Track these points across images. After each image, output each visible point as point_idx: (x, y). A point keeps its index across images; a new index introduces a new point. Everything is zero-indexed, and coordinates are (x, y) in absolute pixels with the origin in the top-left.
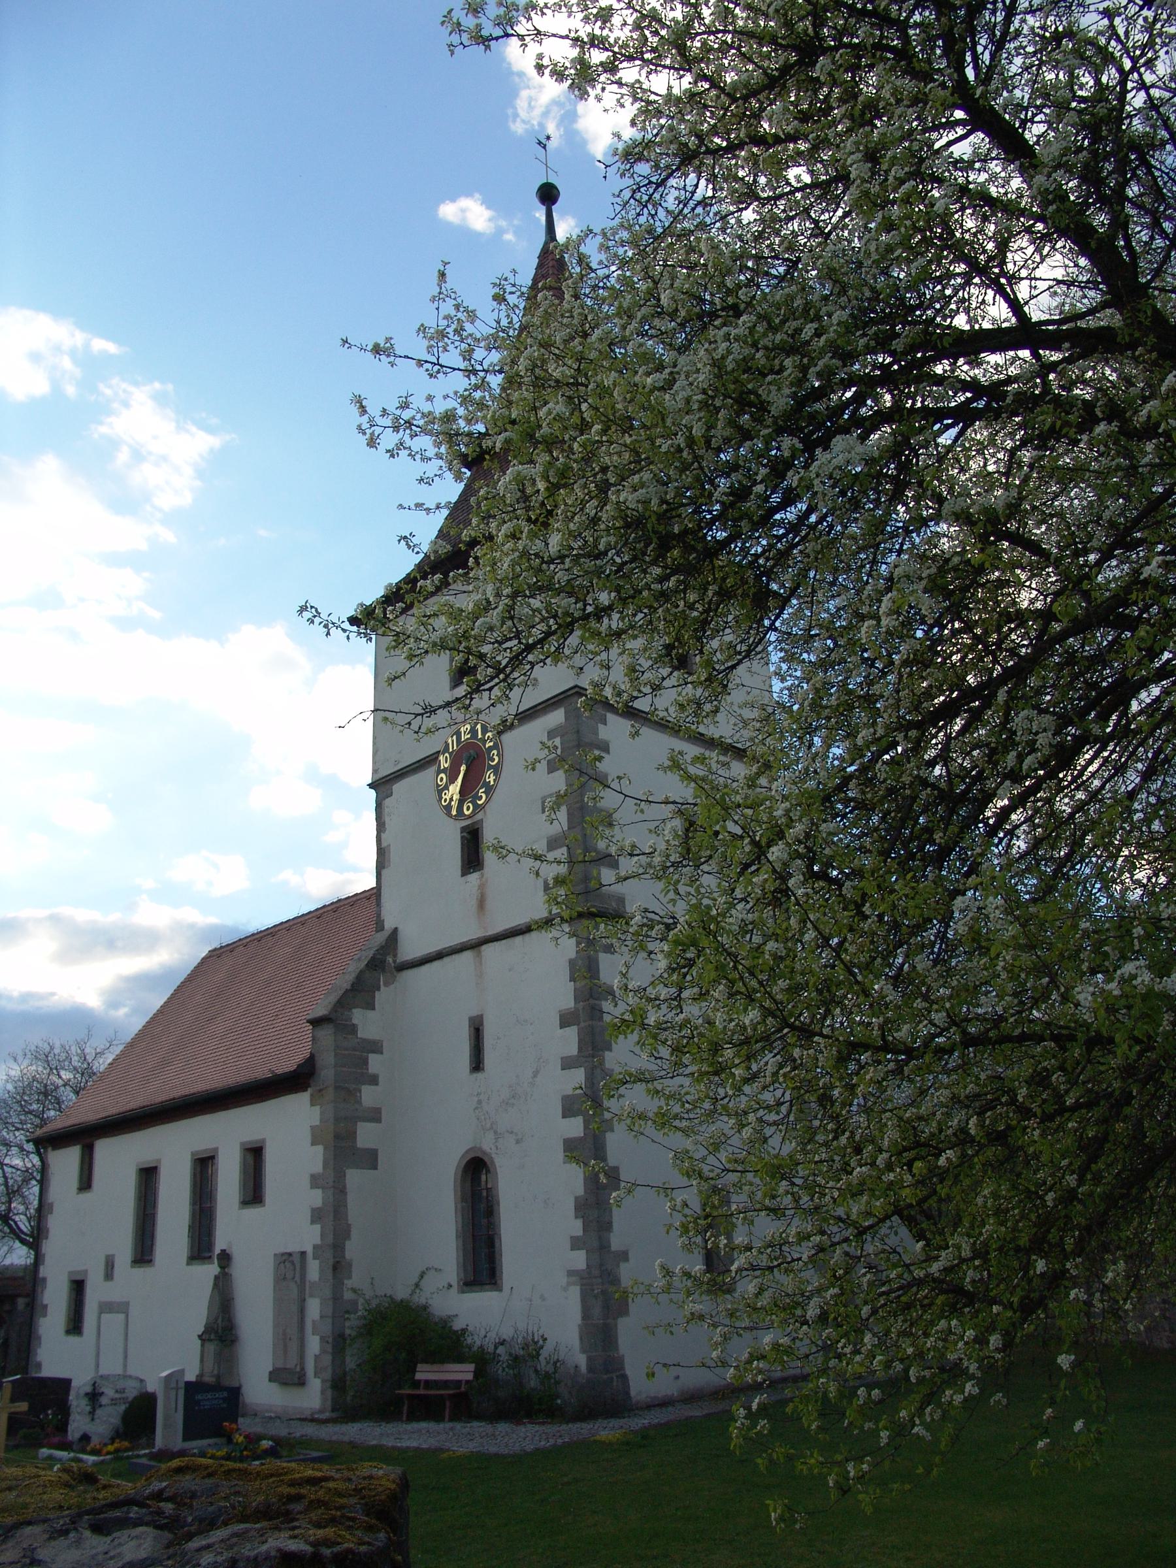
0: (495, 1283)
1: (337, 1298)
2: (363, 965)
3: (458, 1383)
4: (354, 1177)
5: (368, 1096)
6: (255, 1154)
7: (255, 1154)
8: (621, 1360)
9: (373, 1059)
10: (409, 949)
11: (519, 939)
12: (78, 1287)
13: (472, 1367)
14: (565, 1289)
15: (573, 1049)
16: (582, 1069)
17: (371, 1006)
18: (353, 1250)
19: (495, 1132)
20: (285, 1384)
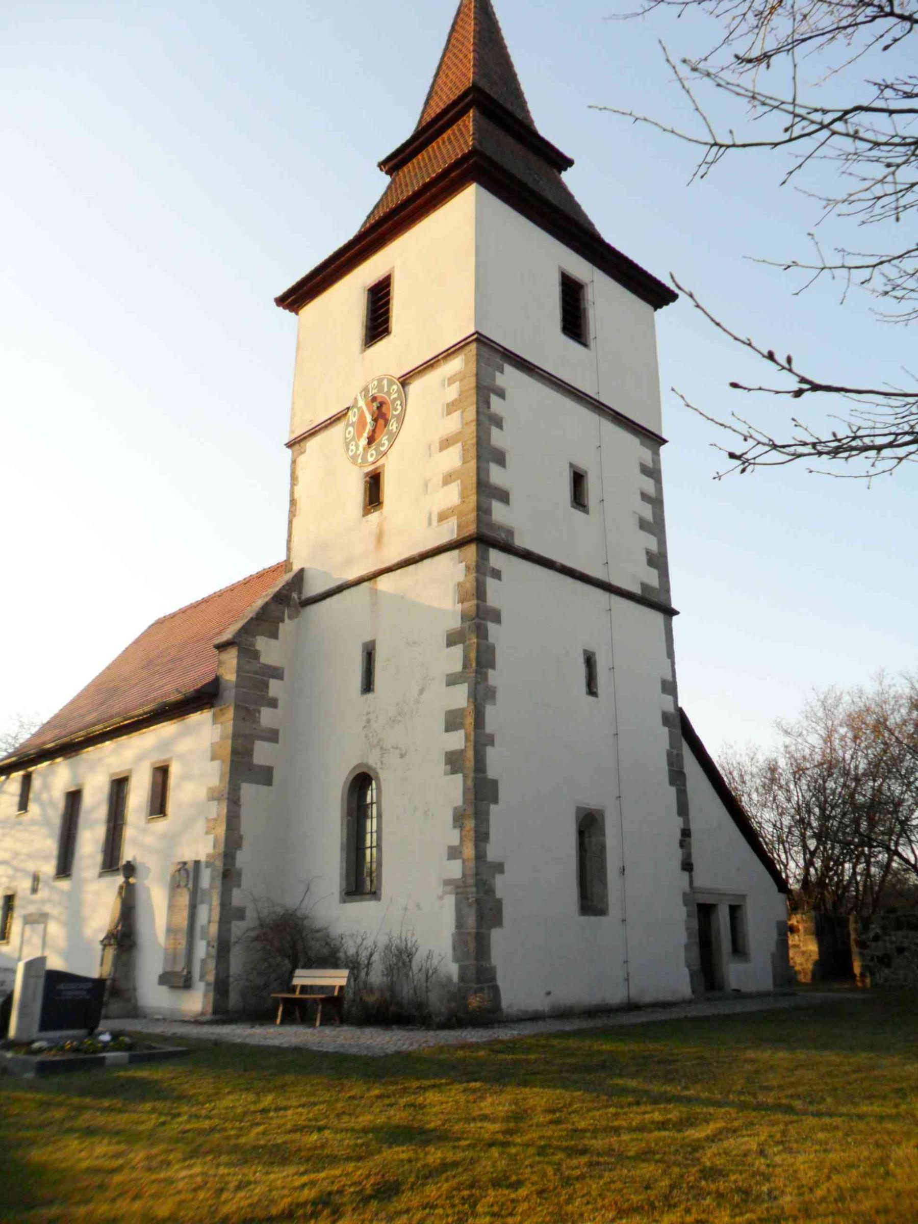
0: (375, 893)
1: (225, 904)
2: (267, 599)
4: (248, 791)
5: (267, 717)
6: (162, 773)
7: (162, 773)
9: (273, 683)
10: (313, 588)
11: (412, 568)
13: (345, 972)
14: (441, 898)
15: (458, 667)
16: (466, 684)
17: (274, 635)
18: (242, 859)
19: (382, 748)
20: (173, 987)
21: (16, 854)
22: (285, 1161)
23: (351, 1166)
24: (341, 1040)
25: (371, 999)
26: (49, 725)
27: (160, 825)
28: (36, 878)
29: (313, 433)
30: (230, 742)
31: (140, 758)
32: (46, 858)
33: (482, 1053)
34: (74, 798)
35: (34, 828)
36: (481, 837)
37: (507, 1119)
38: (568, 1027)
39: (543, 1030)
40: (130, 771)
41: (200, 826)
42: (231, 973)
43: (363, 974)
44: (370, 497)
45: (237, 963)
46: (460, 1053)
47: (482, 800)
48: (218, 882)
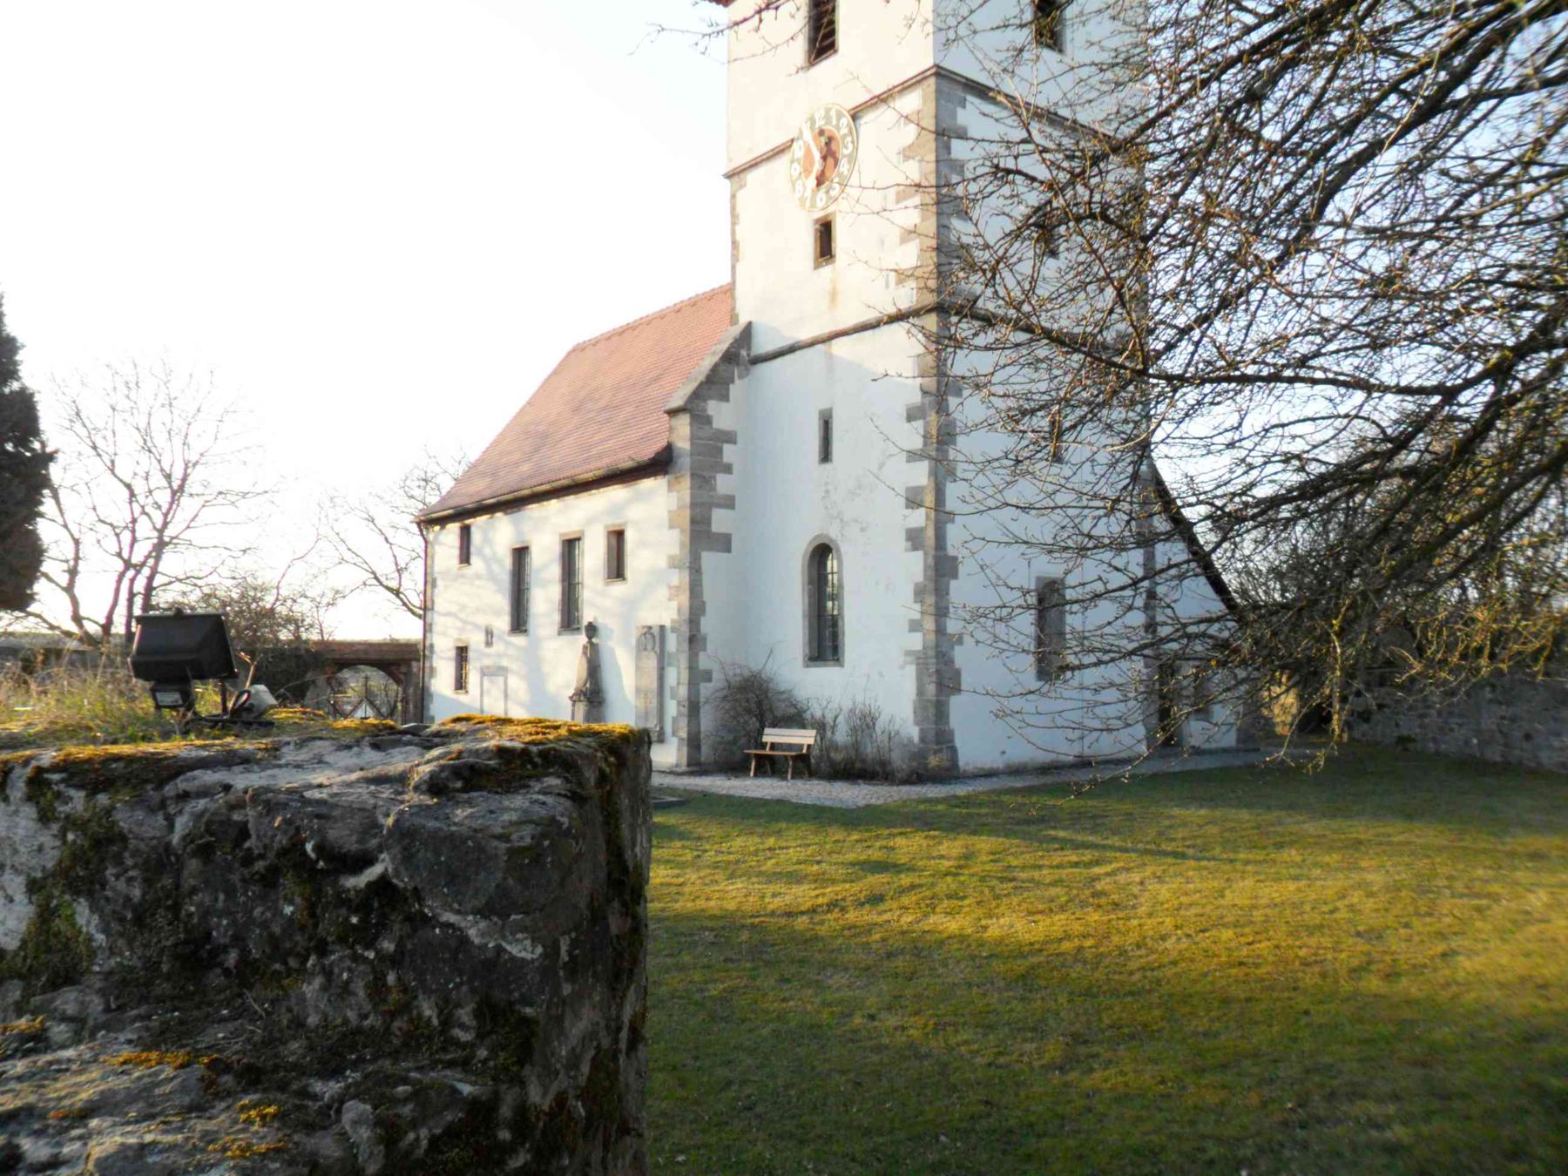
1: (692, 668)
2: (716, 358)
3: (801, 746)
4: (709, 559)
5: (723, 484)
6: (617, 537)
7: (617, 537)
8: (951, 733)
9: (727, 448)
10: (762, 345)
12: (462, 654)
13: (814, 732)
14: (902, 668)
17: (725, 397)
18: (707, 625)
21: (463, 607)
22: (799, 882)
23: (848, 886)
24: (815, 793)
25: (838, 757)
26: (474, 470)
27: (618, 588)
28: (489, 633)
29: (754, 165)
30: (688, 512)
31: (591, 521)
32: (497, 613)
33: (940, 807)
34: (521, 554)
35: (477, 582)
36: (941, 613)
37: (959, 858)
38: (1019, 783)
39: (995, 786)
40: (582, 532)
41: (662, 593)
42: (703, 729)
43: (829, 734)
44: (822, 248)
45: (707, 722)
46: (922, 807)
47: (944, 576)
48: (686, 646)
